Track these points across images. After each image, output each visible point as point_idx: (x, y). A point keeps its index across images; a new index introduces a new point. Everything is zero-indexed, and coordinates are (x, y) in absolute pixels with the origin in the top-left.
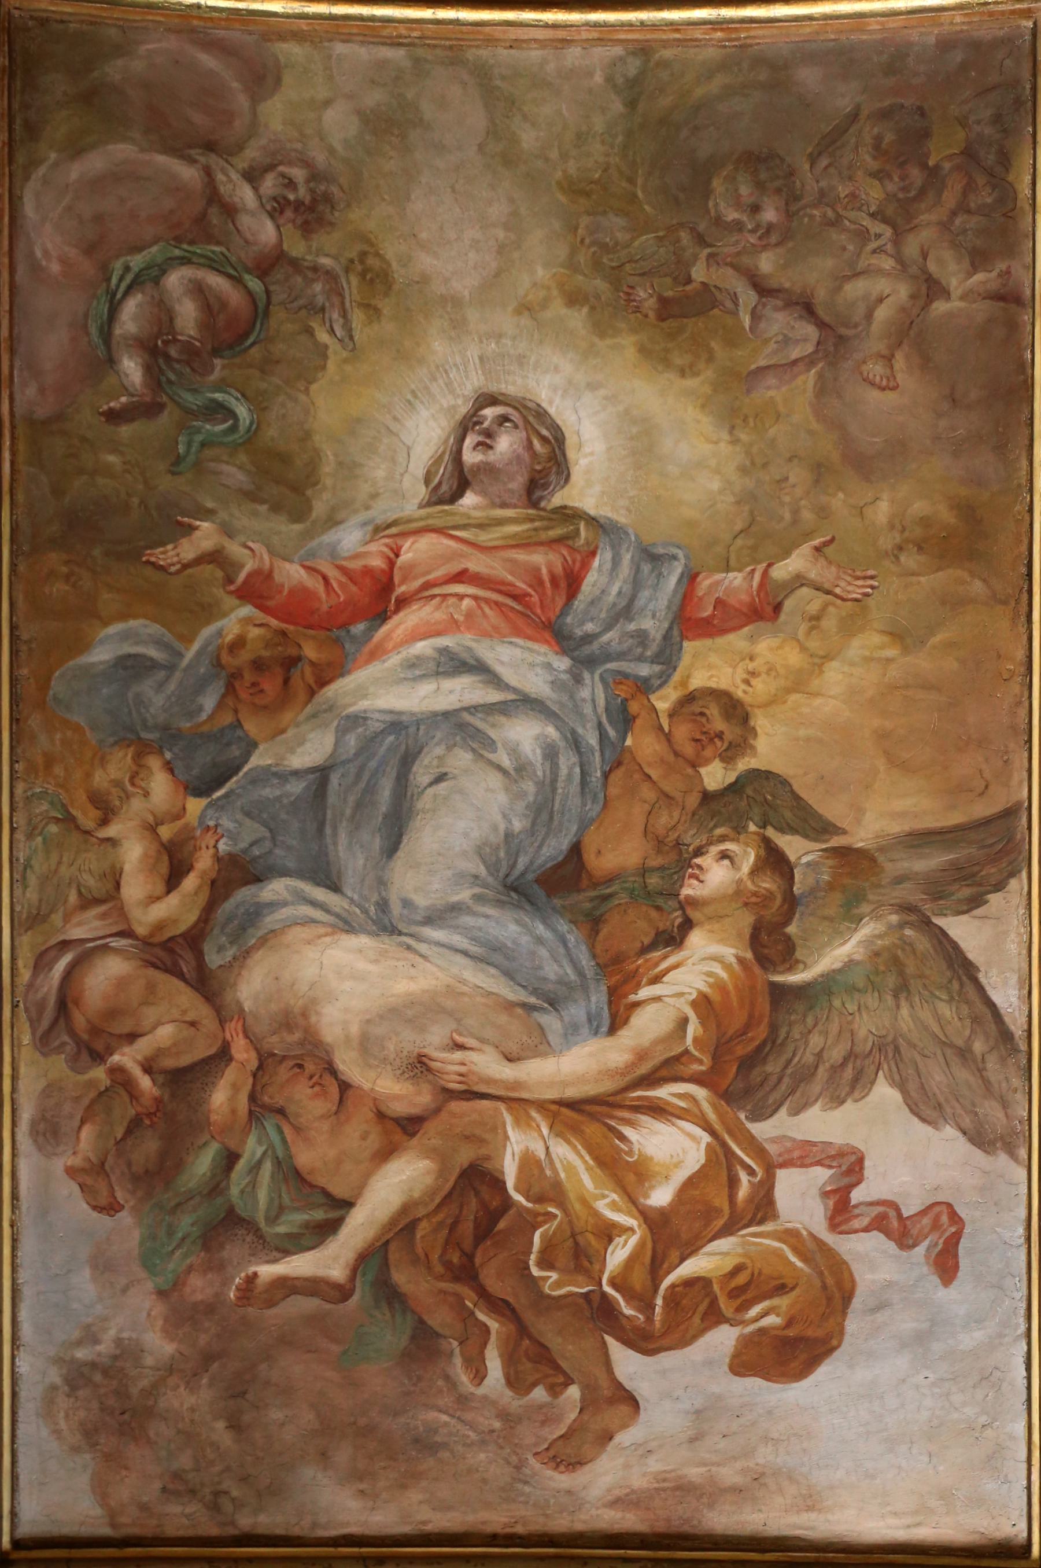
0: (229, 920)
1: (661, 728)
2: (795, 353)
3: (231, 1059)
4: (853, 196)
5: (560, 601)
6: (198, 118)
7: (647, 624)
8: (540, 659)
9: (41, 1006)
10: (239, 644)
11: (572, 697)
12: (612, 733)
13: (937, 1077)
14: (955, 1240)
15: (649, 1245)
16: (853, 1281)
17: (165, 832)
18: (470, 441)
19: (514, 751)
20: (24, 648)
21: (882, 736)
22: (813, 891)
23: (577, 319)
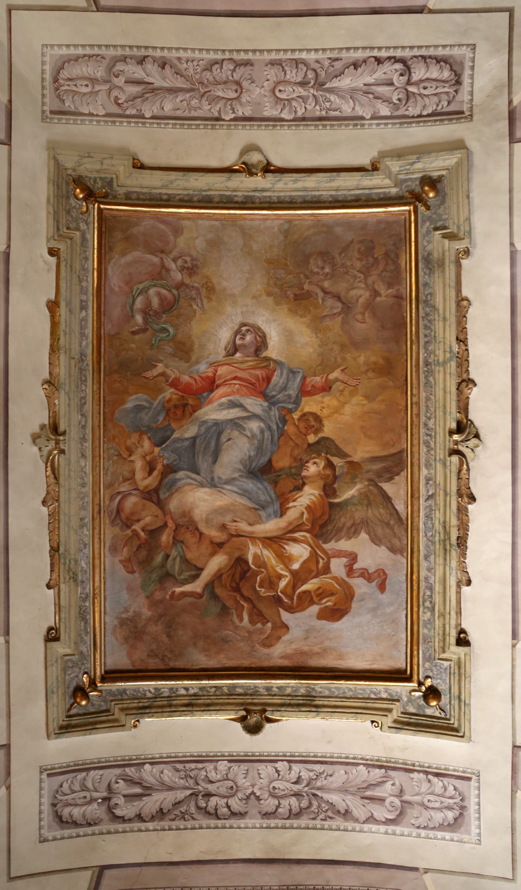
0: (167, 484)
1: (295, 424)
2: (335, 311)
3: (167, 526)
4: (352, 265)
5: (265, 385)
6: (159, 244)
7: (291, 392)
8: (259, 403)
9: (112, 512)
10: (170, 400)
11: (268, 414)
12: (280, 425)
13: (379, 531)
14: (384, 580)
15: (292, 581)
16: (354, 593)
17: (148, 458)
18: (238, 337)
19: (251, 431)
20: (107, 403)
21: (362, 427)
22: (342, 474)
23: (270, 300)
